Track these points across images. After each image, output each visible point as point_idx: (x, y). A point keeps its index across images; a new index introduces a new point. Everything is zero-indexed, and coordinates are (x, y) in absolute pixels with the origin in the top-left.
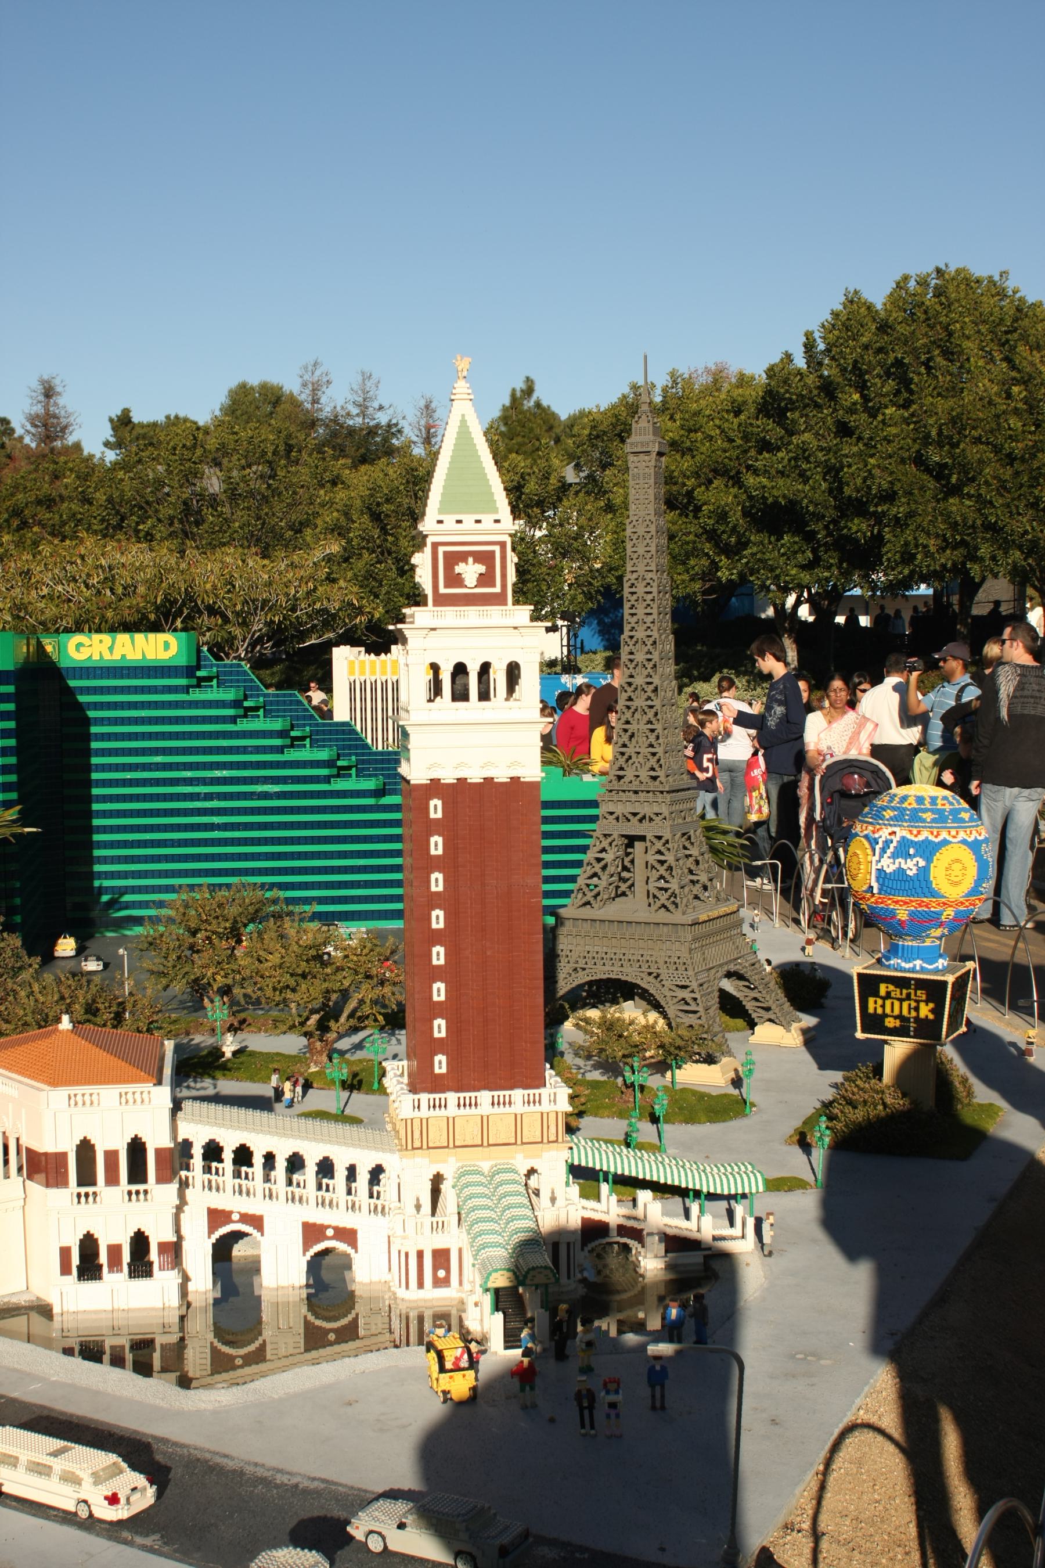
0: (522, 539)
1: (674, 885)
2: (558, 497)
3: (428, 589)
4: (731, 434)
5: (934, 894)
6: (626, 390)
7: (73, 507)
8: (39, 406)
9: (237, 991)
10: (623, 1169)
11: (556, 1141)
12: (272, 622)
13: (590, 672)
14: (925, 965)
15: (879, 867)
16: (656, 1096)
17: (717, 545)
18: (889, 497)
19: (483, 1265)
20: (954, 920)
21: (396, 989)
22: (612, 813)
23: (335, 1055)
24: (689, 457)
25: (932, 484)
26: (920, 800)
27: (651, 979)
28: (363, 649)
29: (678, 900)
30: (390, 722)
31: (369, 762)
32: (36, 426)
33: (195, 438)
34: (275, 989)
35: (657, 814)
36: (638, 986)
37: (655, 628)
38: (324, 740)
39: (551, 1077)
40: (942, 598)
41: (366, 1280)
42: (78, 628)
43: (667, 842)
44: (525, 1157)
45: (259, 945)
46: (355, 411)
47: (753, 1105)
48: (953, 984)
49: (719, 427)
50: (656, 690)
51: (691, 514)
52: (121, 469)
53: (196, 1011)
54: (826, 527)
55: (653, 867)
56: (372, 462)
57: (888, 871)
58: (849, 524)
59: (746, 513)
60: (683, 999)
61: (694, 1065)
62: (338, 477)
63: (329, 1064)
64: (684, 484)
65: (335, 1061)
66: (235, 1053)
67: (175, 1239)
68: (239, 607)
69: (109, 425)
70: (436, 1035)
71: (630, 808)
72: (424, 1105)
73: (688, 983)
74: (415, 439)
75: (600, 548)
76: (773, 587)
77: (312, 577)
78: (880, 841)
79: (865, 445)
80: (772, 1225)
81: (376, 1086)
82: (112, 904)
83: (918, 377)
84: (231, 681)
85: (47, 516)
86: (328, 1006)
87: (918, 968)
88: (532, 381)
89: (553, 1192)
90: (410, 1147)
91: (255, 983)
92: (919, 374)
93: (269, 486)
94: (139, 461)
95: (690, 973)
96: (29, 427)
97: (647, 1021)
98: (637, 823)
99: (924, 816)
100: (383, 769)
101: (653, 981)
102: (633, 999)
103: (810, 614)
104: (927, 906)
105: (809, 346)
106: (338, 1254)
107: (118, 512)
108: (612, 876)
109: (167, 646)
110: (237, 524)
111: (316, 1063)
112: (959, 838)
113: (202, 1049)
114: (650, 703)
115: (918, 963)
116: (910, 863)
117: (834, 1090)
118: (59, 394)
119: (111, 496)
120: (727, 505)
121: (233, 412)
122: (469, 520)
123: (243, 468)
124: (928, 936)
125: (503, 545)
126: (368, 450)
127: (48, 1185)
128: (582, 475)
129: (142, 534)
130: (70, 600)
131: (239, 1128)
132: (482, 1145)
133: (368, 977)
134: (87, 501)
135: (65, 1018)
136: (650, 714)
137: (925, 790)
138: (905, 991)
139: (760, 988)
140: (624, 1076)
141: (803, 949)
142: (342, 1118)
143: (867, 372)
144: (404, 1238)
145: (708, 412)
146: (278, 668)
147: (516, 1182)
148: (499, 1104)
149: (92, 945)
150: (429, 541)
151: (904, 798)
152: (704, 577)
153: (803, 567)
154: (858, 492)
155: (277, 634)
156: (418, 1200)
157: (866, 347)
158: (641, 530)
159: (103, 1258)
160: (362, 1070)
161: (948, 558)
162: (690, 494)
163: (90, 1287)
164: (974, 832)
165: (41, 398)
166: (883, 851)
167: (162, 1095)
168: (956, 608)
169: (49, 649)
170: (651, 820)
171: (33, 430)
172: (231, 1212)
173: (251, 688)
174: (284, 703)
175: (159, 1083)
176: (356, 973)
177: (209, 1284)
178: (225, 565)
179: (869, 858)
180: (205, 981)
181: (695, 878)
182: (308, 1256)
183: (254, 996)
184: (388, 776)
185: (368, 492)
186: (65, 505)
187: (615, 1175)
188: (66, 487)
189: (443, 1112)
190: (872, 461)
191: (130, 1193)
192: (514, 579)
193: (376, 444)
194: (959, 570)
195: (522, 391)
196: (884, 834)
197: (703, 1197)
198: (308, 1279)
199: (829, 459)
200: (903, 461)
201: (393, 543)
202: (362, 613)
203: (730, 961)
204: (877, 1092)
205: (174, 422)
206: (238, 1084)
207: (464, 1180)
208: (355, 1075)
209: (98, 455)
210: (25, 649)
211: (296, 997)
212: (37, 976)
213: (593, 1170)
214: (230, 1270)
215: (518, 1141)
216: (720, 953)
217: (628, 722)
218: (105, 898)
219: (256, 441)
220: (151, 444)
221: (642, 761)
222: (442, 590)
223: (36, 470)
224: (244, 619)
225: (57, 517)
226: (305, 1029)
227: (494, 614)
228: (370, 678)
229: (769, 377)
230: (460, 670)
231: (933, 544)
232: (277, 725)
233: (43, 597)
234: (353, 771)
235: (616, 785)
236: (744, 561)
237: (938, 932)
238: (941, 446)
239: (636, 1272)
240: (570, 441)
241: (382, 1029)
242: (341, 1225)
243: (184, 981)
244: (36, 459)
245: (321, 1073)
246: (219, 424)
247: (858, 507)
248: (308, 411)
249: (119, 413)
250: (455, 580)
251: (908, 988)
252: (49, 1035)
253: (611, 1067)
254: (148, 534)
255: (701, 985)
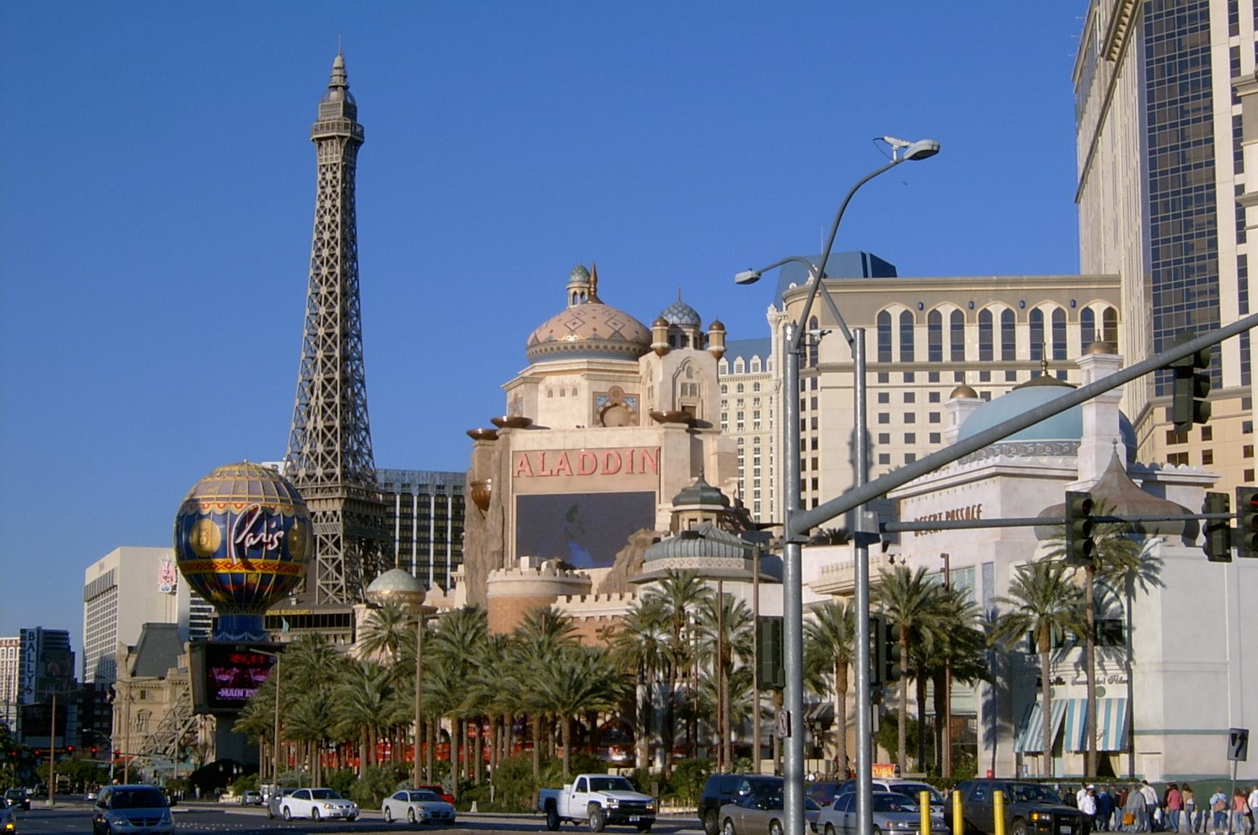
0: (815, 653)
40: (201, 792)
67: (867, 374)
149: (1098, 780)
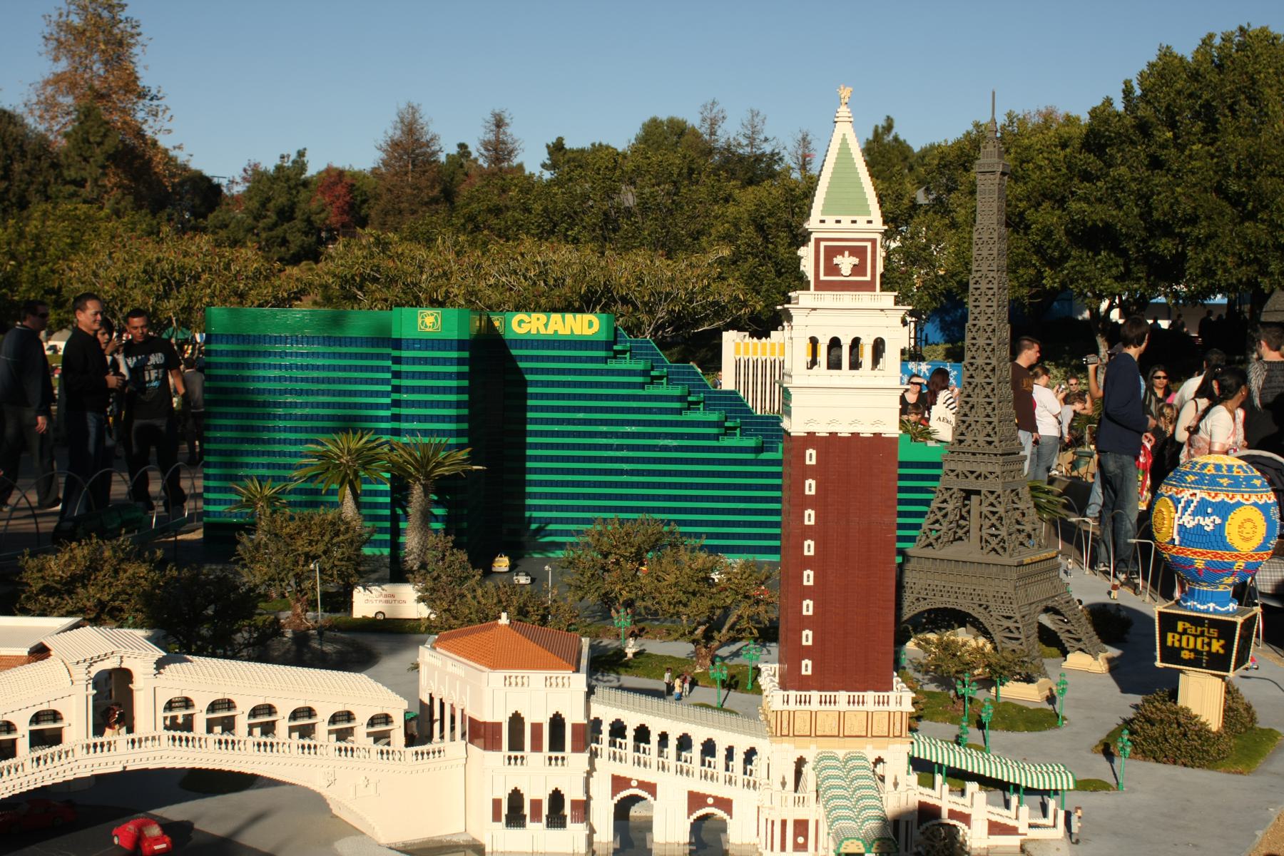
1: (1003, 532)
2: (910, 215)
3: (811, 276)
4: (1057, 164)
5: (1228, 547)
6: (970, 128)
7: (516, 215)
8: (491, 134)
9: (638, 604)
10: (955, 763)
11: (900, 736)
12: (673, 311)
13: (932, 361)
14: (1217, 607)
15: (1181, 522)
16: (983, 705)
17: (1043, 258)
18: (1192, 220)
19: (837, 833)
20: (1245, 570)
21: (770, 608)
22: (953, 471)
23: (718, 659)
24: (1021, 184)
25: (1229, 210)
26: (1218, 467)
27: (981, 609)
28: (747, 334)
29: (1006, 545)
30: (777, 385)
31: (750, 424)
32: (487, 150)
33: (616, 162)
34: (670, 604)
35: (991, 473)
36: (969, 615)
37: (995, 318)
38: (715, 405)
39: (897, 683)
41: (738, 842)
42: (518, 309)
43: (999, 496)
44: (874, 748)
45: (658, 568)
46: (744, 142)
47: (1064, 719)
48: (1242, 625)
49: (1048, 159)
50: (993, 370)
51: (1022, 231)
52: (555, 185)
53: (604, 619)
54: (1137, 246)
55: (986, 517)
56: (758, 184)
57: (1188, 526)
58: (1157, 244)
59: (1068, 232)
60: (1008, 628)
61: (1015, 683)
62: (730, 195)
63: (711, 667)
64: (1017, 206)
65: (717, 664)
66: (635, 654)
67: (585, 798)
68: (646, 299)
69: (545, 151)
70: (804, 643)
71: (969, 467)
72: (792, 700)
73: (1012, 615)
74: (793, 165)
75: (944, 256)
76: (1089, 294)
77: (706, 276)
78: (1183, 501)
79: (1174, 176)
80: (1079, 817)
81: (749, 686)
82: (539, 531)
83: (1224, 120)
84: (641, 354)
85: (495, 221)
86: (713, 619)
87: (1211, 610)
88: (892, 120)
89: (896, 779)
90: (779, 734)
91: (654, 598)
92: (1225, 116)
93: (673, 201)
94: (570, 180)
95: (1014, 606)
96: (483, 151)
97: (977, 643)
98: (974, 480)
99: (1221, 481)
100: (762, 430)
101: (983, 611)
102: (965, 626)
103: (1120, 318)
104: (1221, 558)
105: (1128, 92)
106: (716, 820)
107: (551, 220)
108: (951, 523)
109: (591, 324)
110: (646, 233)
111: (701, 666)
112: (1251, 501)
113: (609, 650)
114: (988, 380)
115: (1212, 605)
116: (1208, 521)
117: (1134, 711)
118: (507, 124)
119: (546, 207)
120: (1052, 225)
121: (646, 141)
122: (846, 221)
123: (654, 186)
124: (1221, 583)
125: (874, 241)
126: (754, 174)
127: (485, 748)
128: (931, 197)
129: (570, 239)
130: (511, 289)
131: (640, 711)
132: (838, 736)
133: (747, 597)
134: (527, 210)
135: (504, 615)
136: (988, 389)
137: (1223, 460)
138: (1199, 629)
139: (1073, 622)
140: (955, 689)
141: (1109, 593)
142: (721, 708)
143: (1178, 114)
144: (771, 809)
145: (1038, 147)
146: (675, 350)
147: (865, 768)
148: (854, 702)
150: (813, 237)
151: (1204, 466)
152: (1030, 284)
153: (1116, 279)
154: (1165, 215)
155: (678, 321)
156: (784, 778)
157: (1179, 93)
158: (985, 237)
159: (527, 810)
160: (739, 673)
161: (1244, 273)
162: (1021, 214)
163: (515, 832)
164: (1265, 497)
165: (493, 128)
166: (1185, 509)
167: (579, 681)
168: (1247, 316)
169: (497, 324)
170: (986, 477)
171: (486, 153)
172: (631, 779)
173: (657, 361)
174: (684, 373)
175: (577, 671)
176: (737, 593)
177: (611, 838)
178: (636, 264)
179: (1172, 515)
180: (613, 595)
181: (1020, 527)
182: (692, 820)
183: (653, 608)
184: (766, 436)
185: (754, 208)
186: (510, 213)
187: (949, 768)
188: (511, 199)
189: (807, 707)
190: (1179, 189)
191: (550, 759)
192: (882, 270)
193: (761, 169)
194: (1253, 284)
195: (883, 127)
196: (1186, 495)
197: (1021, 790)
198: (690, 838)
199: (1141, 189)
200: (1206, 190)
201: (773, 250)
202: (747, 306)
203: (1048, 598)
204: (1173, 713)
205: (598, 149)
206: (637, 679)
207: (822, 764)
208: (733, 677)
209: (537, 174)
210: (478, 324)
211: (687, 610)
212: (480, 584)
213: (930, 762)
214: (628, 825)
215: (868, 735)
216: (1039, 591)
217: (969, 396)
218: (534, 526)
219: (665, 164)
220: (581, 167)
221: (980, 428)
222: (822, 278)
223: (487, 185)
224: (651, 308)
225: (503, 223)
226: (693, 637)
227: (864, 299)
228: (752, 357)
229: (1092, 117)
230: (835, 343)
231: (1230, 262)
232: (677, 391)
233: (490, 286)
234: (738, 431)
235: (957, 448)
236: (1066, 272)
237: (1230, 580)
238: (1238, 176)
239: (963, 850)
240: (922, 170)
241: (756, 640)
242: (720, 796)
243: (597, 594)
244: (488, 176)
245: (705, 674)
246: (635, 150)
247: (1165, 229)
248: (706, 142)
249: (554, 141)
250: (833, 269)
251: (1202, 626)
252: (491, 628)
253: (945, 681)
254: (575, 238)
255: (1023, 617)
